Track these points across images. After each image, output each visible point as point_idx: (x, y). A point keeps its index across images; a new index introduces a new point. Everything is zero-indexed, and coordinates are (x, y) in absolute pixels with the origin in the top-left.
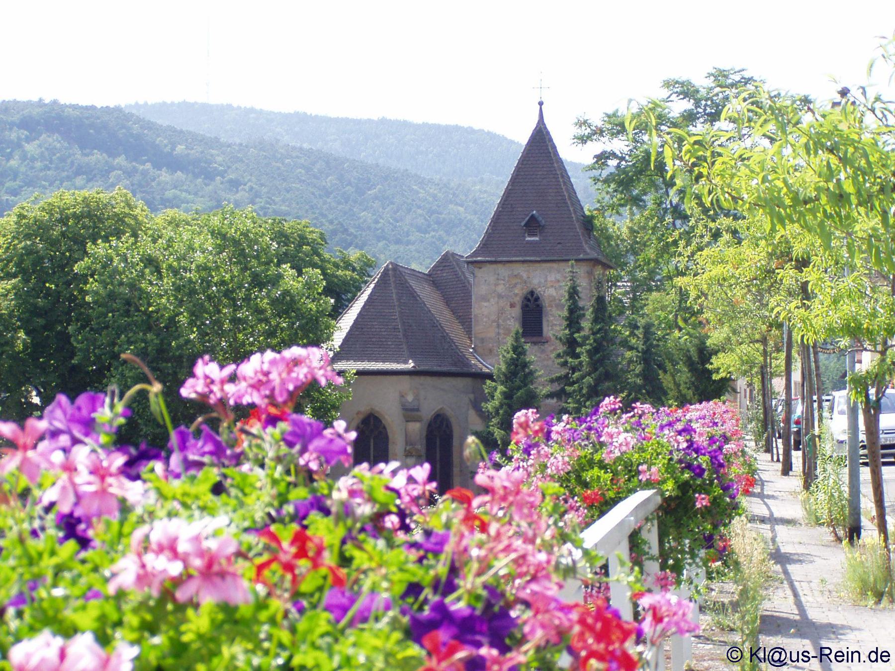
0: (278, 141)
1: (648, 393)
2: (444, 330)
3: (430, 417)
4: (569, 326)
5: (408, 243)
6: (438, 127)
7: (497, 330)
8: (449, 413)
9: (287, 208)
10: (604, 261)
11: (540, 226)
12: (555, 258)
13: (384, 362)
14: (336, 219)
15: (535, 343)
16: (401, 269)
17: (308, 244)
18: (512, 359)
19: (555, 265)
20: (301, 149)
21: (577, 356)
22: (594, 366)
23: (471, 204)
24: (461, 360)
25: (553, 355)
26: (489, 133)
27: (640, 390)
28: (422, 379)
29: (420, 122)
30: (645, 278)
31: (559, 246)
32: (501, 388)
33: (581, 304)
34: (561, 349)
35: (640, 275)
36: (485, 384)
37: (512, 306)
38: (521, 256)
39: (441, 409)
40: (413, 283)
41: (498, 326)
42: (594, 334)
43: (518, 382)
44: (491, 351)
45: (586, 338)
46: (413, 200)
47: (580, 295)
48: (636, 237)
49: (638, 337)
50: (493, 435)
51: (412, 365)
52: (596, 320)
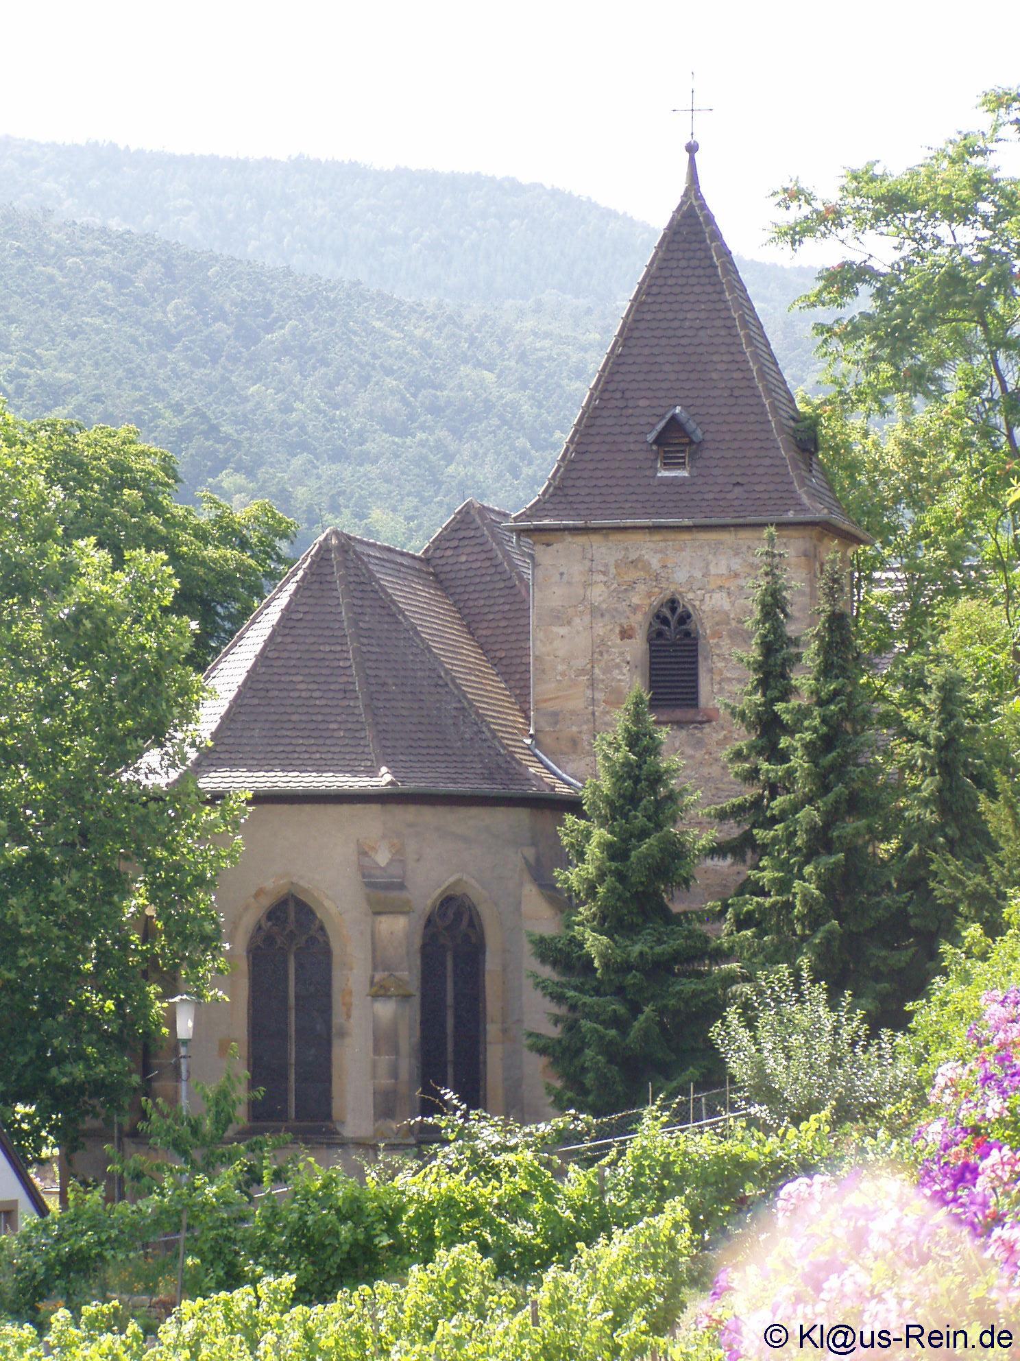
0: (48, 213)
1: (951, 842)
2: (464, 693)
3: (429, 902)
4: (763, 684)
5: (364, 458)
6: (430, 179)
7: (589, 693)
8: (477, 893)
9: (71, 377)
10: (846, 526)
11: (692, 442)
12: (728, 520)
13: (319, 770)
14: (190, 401)
15: (680, 724)
16: (359, 548)
17: (133, 485)
18: (627, 763)
19: (727, 537)
20: (104, 230)
21: (782, 757)
22: (823, 782)
23: (513, 363)
24: (508, 767)
25: (724, 754)
26: (554, 193)
27: (931, 836)
28: (410, 813)
29: (390, 166)
30: (938, 562)
31: (738, 490)
32: (600, 834)
33: (791, 630)
34: (743, 738)
35: (930, 556)
36: (562, 823)
37: (626, 634)
38: (648, 515)
39: (459, 881)
40: (387, 580)
41: (592, 684)
42: (821, 703)
43: (640, 820)
44: (574, 743)
45: (804, 713)
46: (375, 356)
47: (789, 610)
48: (920, 465)
49: (927, 711)
50: (581, 945)
51: (388, 778)
52: (826, 671)
